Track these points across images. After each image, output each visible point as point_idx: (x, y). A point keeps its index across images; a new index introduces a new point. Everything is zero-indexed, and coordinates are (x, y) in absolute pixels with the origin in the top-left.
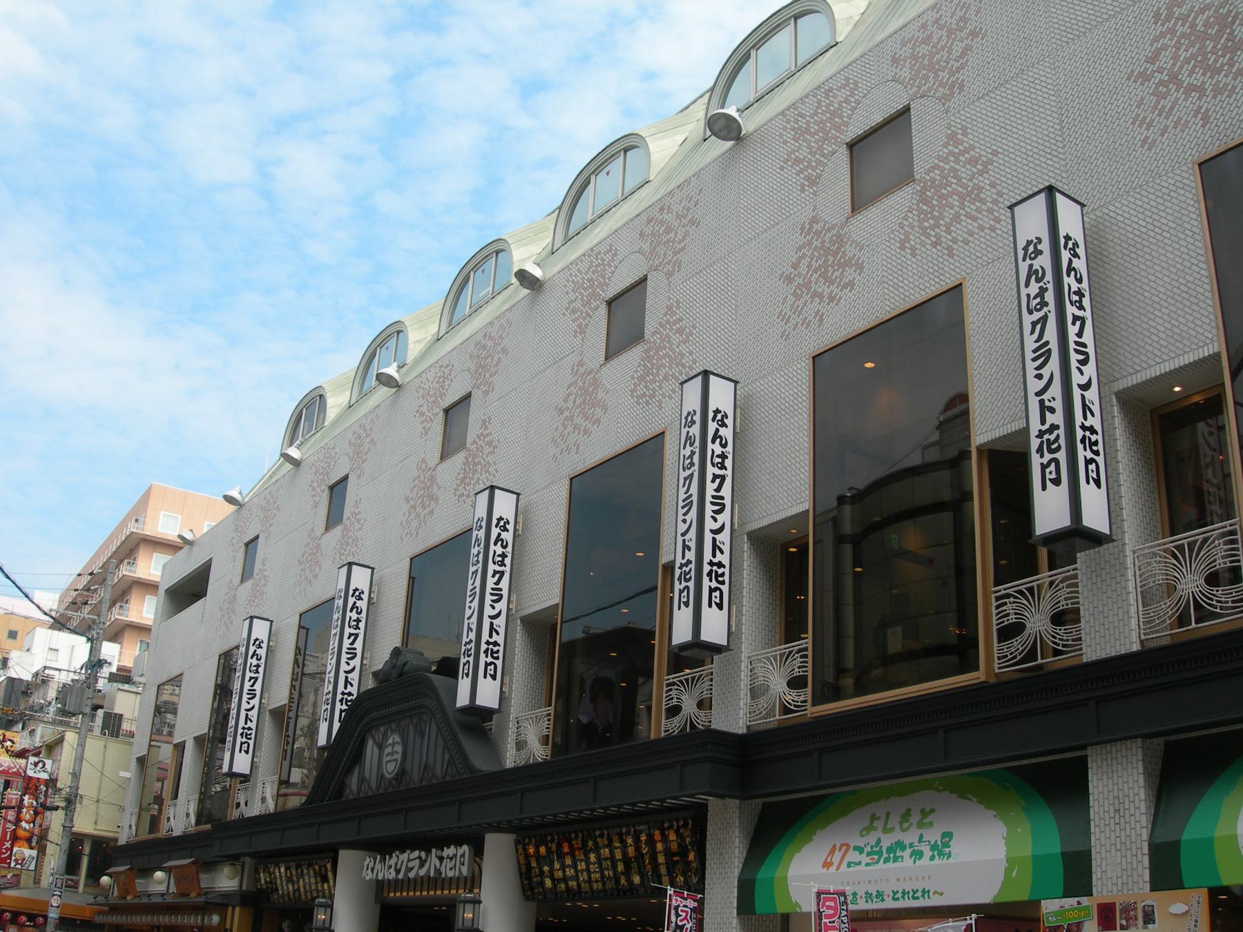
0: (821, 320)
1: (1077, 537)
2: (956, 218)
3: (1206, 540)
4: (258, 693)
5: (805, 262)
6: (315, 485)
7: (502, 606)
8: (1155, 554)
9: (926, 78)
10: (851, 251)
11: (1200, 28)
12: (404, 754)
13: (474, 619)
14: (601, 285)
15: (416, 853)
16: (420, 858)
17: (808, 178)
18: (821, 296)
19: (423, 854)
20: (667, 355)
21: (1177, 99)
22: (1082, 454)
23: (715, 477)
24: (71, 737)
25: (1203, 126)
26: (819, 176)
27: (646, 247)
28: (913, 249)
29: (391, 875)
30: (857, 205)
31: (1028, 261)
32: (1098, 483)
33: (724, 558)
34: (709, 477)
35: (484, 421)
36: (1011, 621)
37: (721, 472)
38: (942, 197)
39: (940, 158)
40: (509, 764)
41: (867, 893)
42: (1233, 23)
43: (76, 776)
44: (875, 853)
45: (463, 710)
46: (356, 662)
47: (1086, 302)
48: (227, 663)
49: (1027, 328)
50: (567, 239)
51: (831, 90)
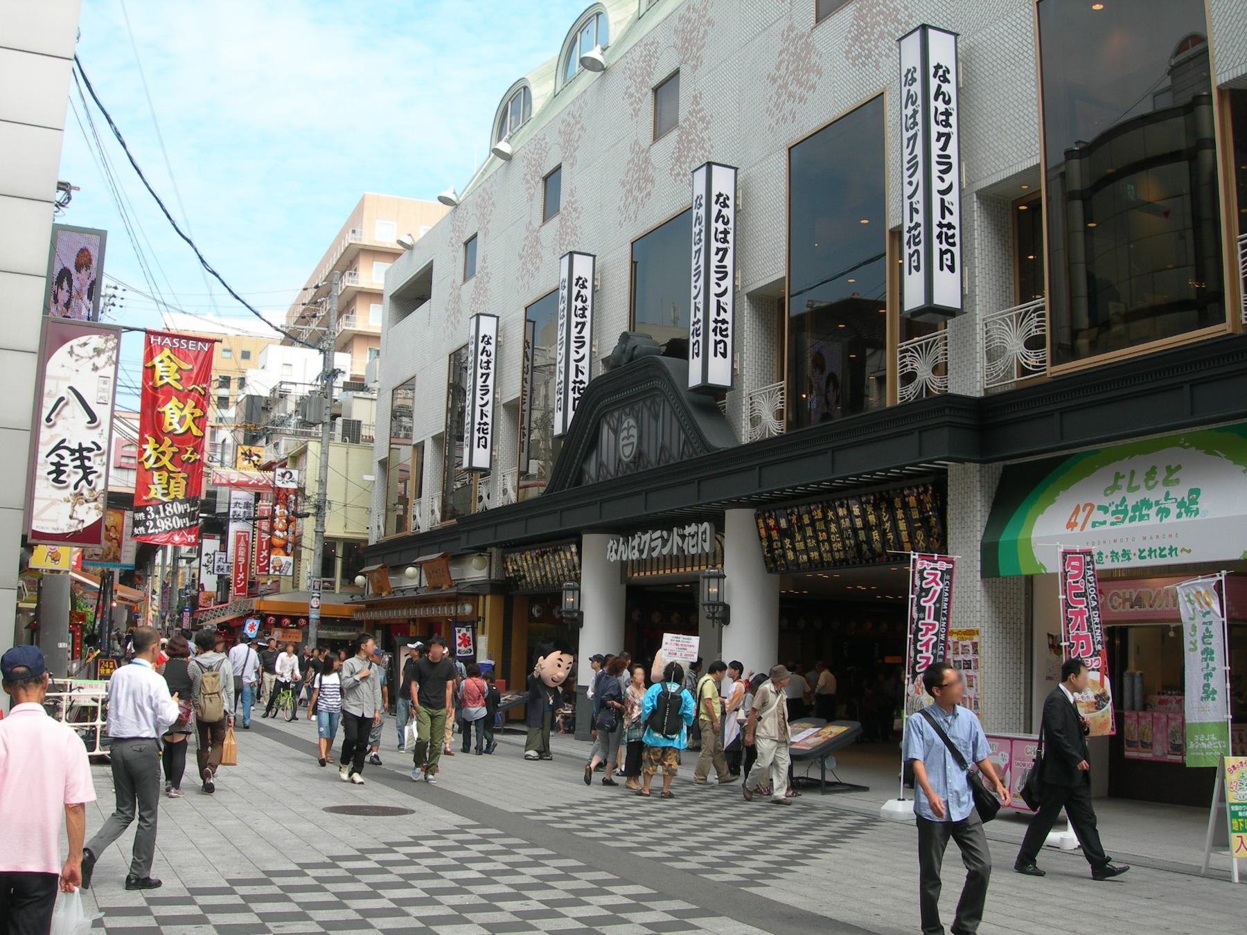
4: (491, 388)
6: (529, 177)
12: (640, 437)
13: (701, 298)
15: (658, 534)
16: (662, 537)
20: (881, 12)
23: (940, 135)
24: (314, 447)
29: (635, 555)
33: (954, 219)
34: (479, 375)
35: (695, 97)
40: (745, 440)
43: (322, 483)
45: (696, 390)
48: (457, 362)
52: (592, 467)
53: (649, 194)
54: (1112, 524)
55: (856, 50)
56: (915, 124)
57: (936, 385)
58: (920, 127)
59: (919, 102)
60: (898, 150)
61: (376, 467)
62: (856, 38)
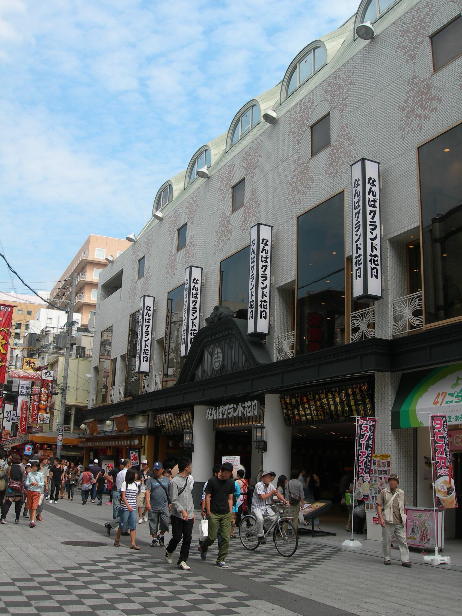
0: (421, 129)
3: (413, 298)
6: (171, 229)
7: (267, 282)
10: (434, 92)
12: (223, 358)
14: (307, 119)
15: (232, 406)
16: (234, 407)
17: (410, 56)
18: (420, 116)
19: (235, 406)
26: (415, 54)
27: (329, 97)
29: (220, 416)
30: (436, 69)
34: (260, 266)
40: (275, 360)
41: (456, 416)
43: (65, 377)
45: (251, 335)
46: (197, 314)
48: (134, 319)
50: (287, 97)
51: (419, 9)
52: (199, 372)
53: (229, 238)
56: (359, 206)
57: (369, 334)
58: (361, 208)
59: (361, 195)
62: (331, 164)
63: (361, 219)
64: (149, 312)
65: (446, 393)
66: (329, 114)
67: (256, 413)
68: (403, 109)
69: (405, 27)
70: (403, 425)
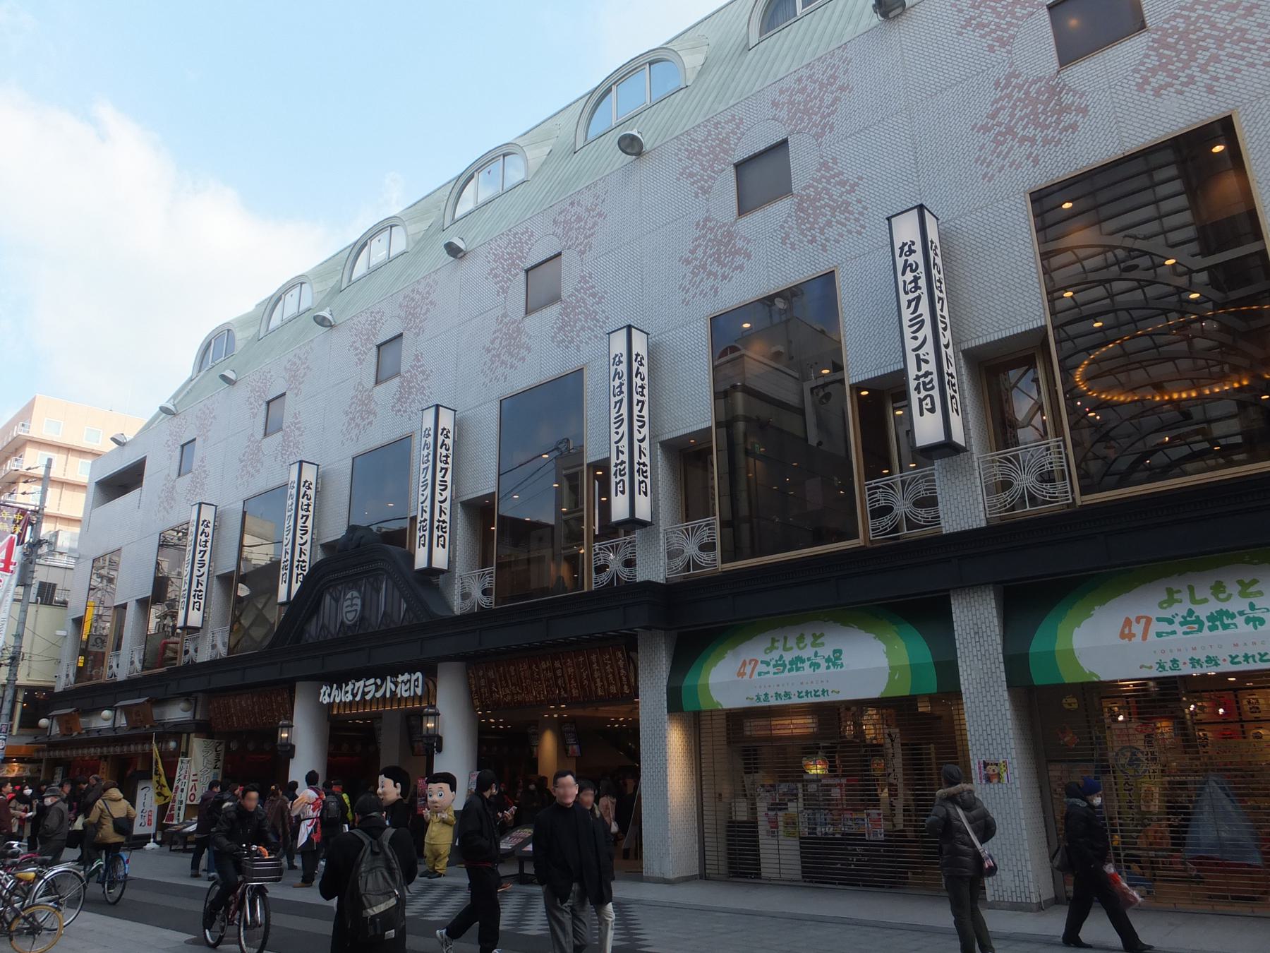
0: (716, 292)
1: (633, 523)
2: (829, 223)
4: (207, 562)
5: (498, 341)
6: (252, 400)
8: (993, 461)
9: (802, 119)
10: (740, 244)
11: (1033, 94)
12: (363, 605)
13: (290, 546)
14: (519, 258)
15: (372, 681)
16: (375, 683)
17: (702, 188)
18: (715, 275)
20: (581, 313)
21: (1012, 147)
22: (637, 478)
23: (639, 402)
25: (1034, 167)
26: (710, 187)
27: (559, 231)
28: (793, 245)
30: (742, 211)
31: (904, 257)
32: (646, 494)
33: (446, 518)
34: (438, 469)
35: (417, 356)
36: (883, 507)
37: (641, 398)
38: (816, 208)
39: (813, 179)
40: (457, 611)
41: (1192, 659)
42: (1060, 92)
44: (780, 665)
45: (421, 571)
46: (205, 569)
47: (646, 392)
49: (613, 405)
51: (719, 123)
53: (370, 423)
54: (1185, 633)
55: (560, 336)
56: (621, 392)
57: (625, 573)
58: (625, 394)
59: (625, 377)
60: (420, 473)
61: (70, 626)
62: (561, 328)
63: (624, 410)
64: (309, 492)
65: (1149, 620)
66: (401, 335)
67: (419, 691)
68: (688, 262)
69: (695, 146)
70: (688, 706)
